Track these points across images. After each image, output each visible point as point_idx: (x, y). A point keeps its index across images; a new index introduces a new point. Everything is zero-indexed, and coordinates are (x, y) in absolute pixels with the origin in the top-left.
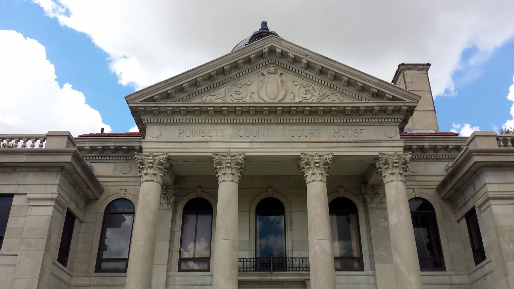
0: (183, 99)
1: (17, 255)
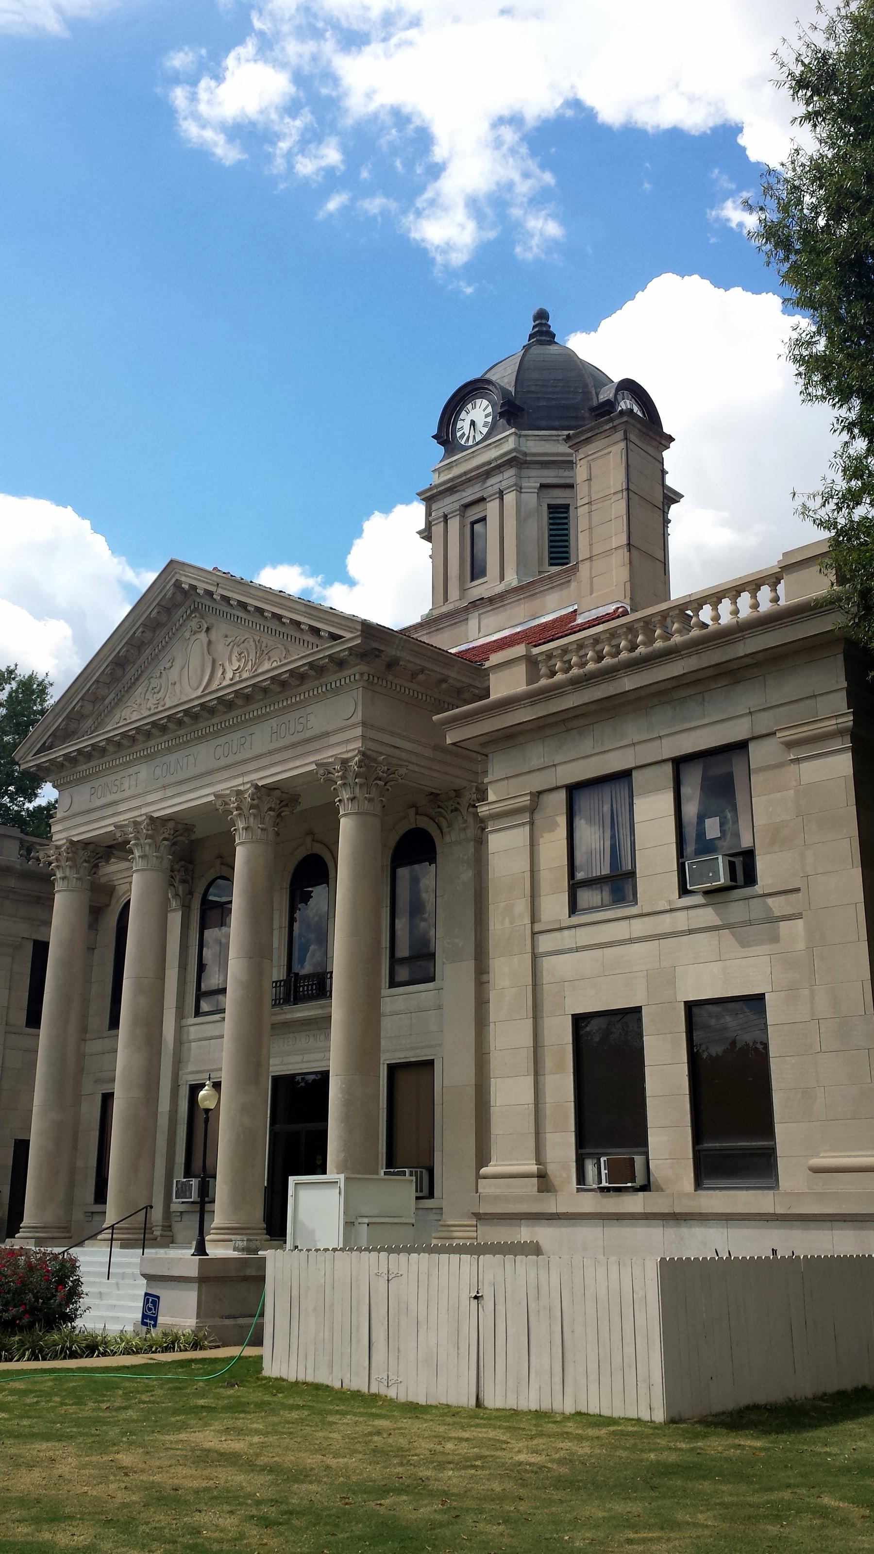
1: (797, 890)
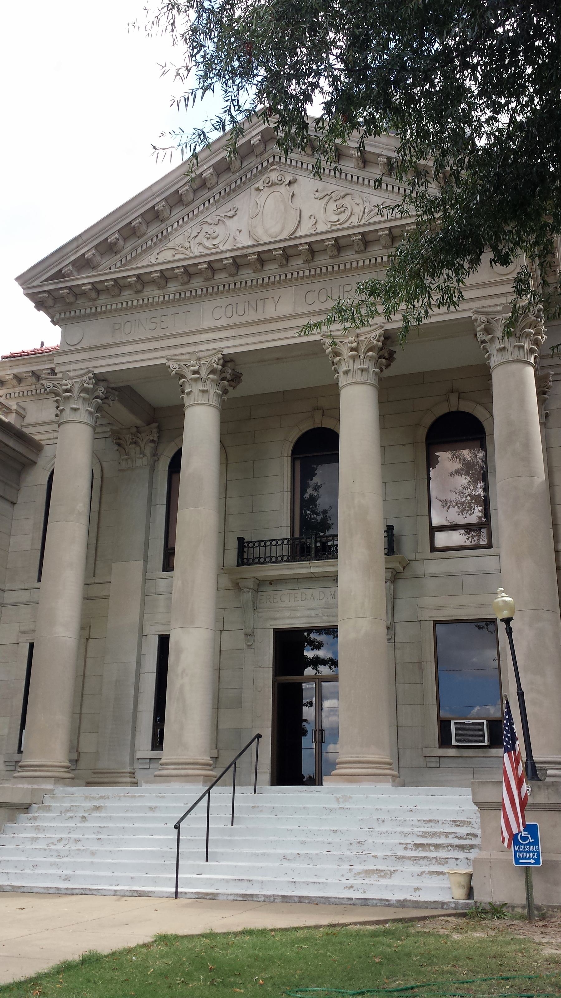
0: (116, 265)
